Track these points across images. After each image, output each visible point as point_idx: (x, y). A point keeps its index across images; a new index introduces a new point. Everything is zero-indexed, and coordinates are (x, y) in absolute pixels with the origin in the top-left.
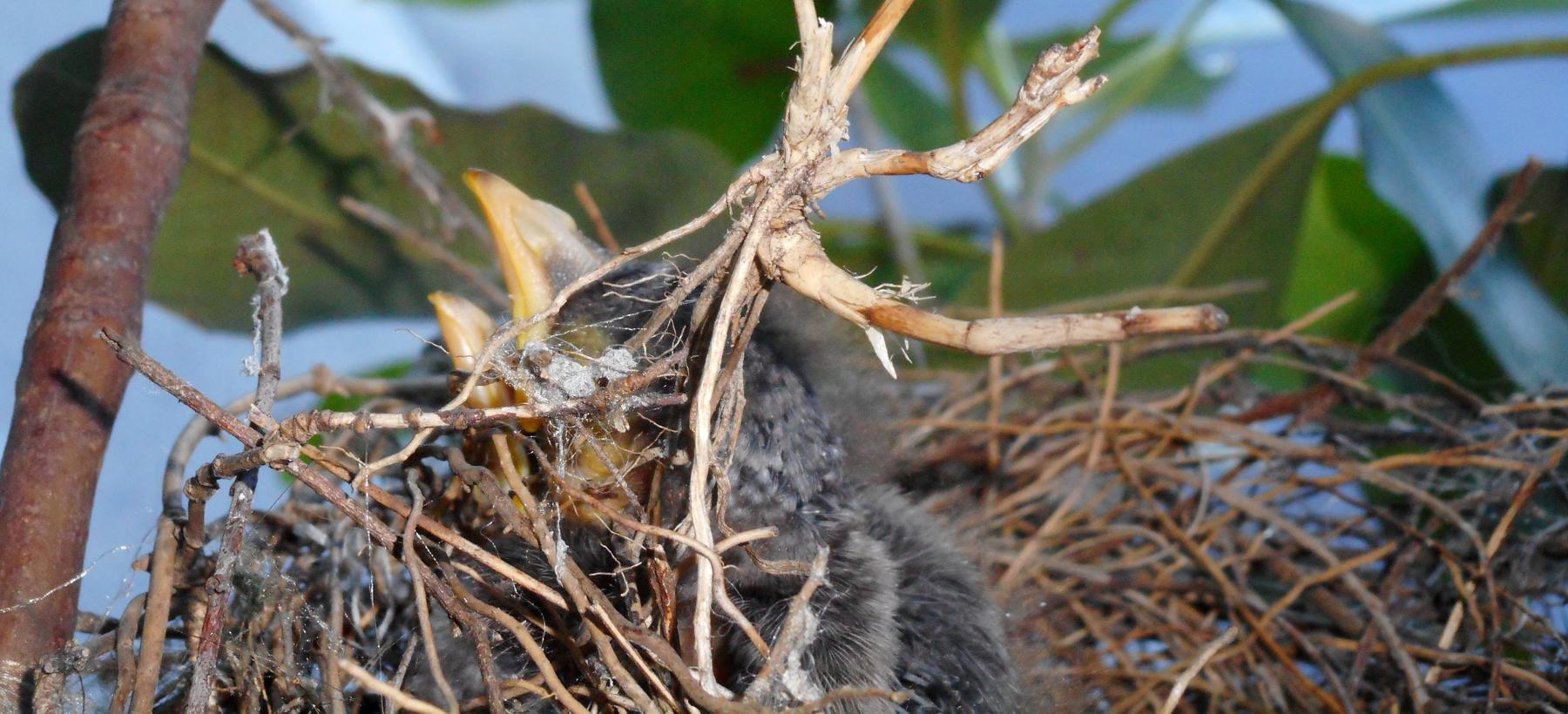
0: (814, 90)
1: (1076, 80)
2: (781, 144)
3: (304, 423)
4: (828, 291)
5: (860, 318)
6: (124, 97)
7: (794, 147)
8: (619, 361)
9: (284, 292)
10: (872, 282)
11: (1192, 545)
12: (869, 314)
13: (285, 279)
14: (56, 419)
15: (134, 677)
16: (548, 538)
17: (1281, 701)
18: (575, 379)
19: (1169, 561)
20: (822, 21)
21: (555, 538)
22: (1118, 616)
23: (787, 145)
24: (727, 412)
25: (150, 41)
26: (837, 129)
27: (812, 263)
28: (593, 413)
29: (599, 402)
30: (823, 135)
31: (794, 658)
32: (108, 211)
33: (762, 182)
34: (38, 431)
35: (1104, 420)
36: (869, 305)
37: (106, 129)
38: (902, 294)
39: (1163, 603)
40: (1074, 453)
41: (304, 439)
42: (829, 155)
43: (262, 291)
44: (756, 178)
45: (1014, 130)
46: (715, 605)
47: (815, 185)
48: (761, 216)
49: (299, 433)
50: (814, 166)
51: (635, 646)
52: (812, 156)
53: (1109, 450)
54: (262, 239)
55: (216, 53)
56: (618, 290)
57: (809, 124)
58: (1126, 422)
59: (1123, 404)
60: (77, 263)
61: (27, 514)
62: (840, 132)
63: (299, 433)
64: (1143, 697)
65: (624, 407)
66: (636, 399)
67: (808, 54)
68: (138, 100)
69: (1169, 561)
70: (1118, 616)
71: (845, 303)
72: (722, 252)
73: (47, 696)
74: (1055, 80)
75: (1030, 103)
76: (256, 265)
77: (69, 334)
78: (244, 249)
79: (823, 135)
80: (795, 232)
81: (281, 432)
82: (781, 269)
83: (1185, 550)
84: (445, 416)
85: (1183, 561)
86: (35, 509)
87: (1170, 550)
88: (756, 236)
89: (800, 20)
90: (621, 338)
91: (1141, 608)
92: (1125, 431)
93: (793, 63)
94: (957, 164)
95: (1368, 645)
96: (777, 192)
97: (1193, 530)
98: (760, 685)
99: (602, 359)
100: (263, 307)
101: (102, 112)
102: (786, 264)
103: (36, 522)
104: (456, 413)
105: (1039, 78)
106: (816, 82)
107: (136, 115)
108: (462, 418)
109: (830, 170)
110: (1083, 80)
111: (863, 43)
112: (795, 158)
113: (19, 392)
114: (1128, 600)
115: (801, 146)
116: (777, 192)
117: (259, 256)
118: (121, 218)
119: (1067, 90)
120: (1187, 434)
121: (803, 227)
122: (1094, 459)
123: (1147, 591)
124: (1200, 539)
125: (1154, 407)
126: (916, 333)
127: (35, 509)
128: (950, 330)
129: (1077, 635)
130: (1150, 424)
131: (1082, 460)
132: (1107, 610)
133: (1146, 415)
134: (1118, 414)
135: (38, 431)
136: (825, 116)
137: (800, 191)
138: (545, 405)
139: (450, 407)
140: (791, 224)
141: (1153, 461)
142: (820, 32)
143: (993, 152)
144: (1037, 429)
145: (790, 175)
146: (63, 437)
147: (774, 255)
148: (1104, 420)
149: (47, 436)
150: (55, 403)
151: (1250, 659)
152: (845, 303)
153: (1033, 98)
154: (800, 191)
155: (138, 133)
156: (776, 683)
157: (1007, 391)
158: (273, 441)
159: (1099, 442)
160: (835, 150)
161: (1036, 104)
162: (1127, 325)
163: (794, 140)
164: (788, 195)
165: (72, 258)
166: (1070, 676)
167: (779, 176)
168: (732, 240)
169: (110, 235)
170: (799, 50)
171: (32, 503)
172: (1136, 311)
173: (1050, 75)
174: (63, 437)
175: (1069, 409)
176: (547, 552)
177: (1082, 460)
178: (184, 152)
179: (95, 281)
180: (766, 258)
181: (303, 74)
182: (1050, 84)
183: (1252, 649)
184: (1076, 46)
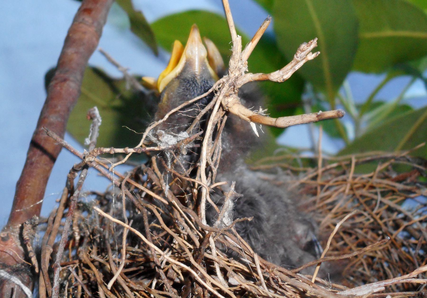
0: (236, 55)
1: (311, 53)
2: (228, 72)
3: (96, 151)
4: (240, 112)
5: (248, 119)
6: (62, 75)
7: (232, 73)
8: (184, 135)
9: (99, 124)
10: (252, 110)
11: (375, 216)
12: (250, 118)
13: (100, 120)
14: (37, 160)
15: (52, 227)
16: (164, 184)
17: (397, 259)
18: (172, 141)
19: (368, 220)
20: (238, 36)
21: (166, 185)
22: (354, 237)
23: (230, 72)
24: (216, 152)
25: (70, 60)
26: (244, 68)
27: (236, 105)
28: (177, 150)
29: (178, 146)
30: (240, 69)
31: (226, 214)
32: (56, 106)
33: (223, 83)
34: (32, 164)
35: (350, 180)
36: (251, 115)
37: (57, 84)
38: (259, 113)
39: (367, 233)
40: (341, 190)
41: (96, 156)
42: (242, 75)
43: (93, 123)
44: (221, 82)
45: (293, 67)
46: (207, 201)
47: (237, 83)
48: (222, 92)
49: (95, 154)
50: (237, 78)
51: (185, 213)
52: (237, 75)
53: (352, 189)
54: (95, 110)
55: (98, 72)
56: (182, 113)
57: (235, 65)
58: (356, 180)
59: (356, 175)
60: (46, 120)
61: (27, 185)
62: (245, 68)
63: (95, 154)
64: (360, 260)
65: (185, 147)
66: (188, 145)
67: (234, 45)
68: (66, 76)
69: (368, 220)
70: (354, 237)
71: (244, 115)
72: (212, 103)
73: (27, 230)
74: (304, 52)
75: (297, 59)
76: (92, 116)
77: (42, 138)
78: (90, 112)
79: (240, 69)
80: (232, 97)
81: (90, 154)
82: (228, 107)
83: (372, 217)
84: (135, 150)
85: (372, 220)
86: (29, 184)
87: (368, 217)
88: (221, 98)
89: (232, 35)
90: (186, 129)
91: (360, 234)
92: (356, 184)
93: (231, 48)
94: (277, 76)
95: (421, 241)
96: (227, 85)
97: (375, 211)
98: (218, 222)
99: (179, 135)
100: (93, 127)
101: (56, 79)
102: (229, 106)
103: (29, 188)
104: (138, 148)
105: (299, 51)
106: (237, 53)
107: (65, 80)
108: (139, 150)
109: (242, 79)
110: (313, 53)
111: (251, 43)
112: (232, 75)
113: (28, 153)
114: (356, 232)
115: (233, 72)
116: (227, 85)
117: (94, 114)
118: (59, 108)
119: (308, 56)
120: (375, 185)
121: (234, 96)
122: (347, 191)
123: (362, 229)
124: (377, 214)
125: (365, 176)
126: (263, 122)
127: (29, 184)
128: (272, 120)
129: (341, 243)
130: (364, 181)
131: (344, 191)
132: (350, 234)
133: (362, 179)
134: (354, 178)
135: (32, 164)
136: (240, 63)
137: (233, 85)
138: (162, 147)
139: (137, 147)
140: (231, 94)
141: (364, 191)
142: (237, 38)
143: (287, 73)
144: (331, 183)
145: (230, 80)
146: (39, 165)
147: (226, 103)
148: (350, 180)
149: (34, 165)
150: (37, 156)
151: (390, 248)
152: (244, 115)
153: (298, 58)
154: (233, 85)
155: (65, 85)
156: (222, 221)
157: (323, 172)
158: (88, 156)
159: (348, 187)
160: (243, 73)
161: (299, 59)
162: (318, 116)
163: (232, 70)
164: (230, 86)
165: (45, 118)
166: (223, 141)
167: (227, 81)
168: (214, 99)
169: (56, 112)
170: (232, 44)
171: (29, 182)
172: (320, 112)
173: (303, 51)
174: (39, 165)
175: (341, 178)
176: (163, 188)
177: (344, 191)
178: (79, 91)
179: (51, 124)
180: (224, 104)
181: (124, 80)
182: (303, 54)
183: (390, 245)
184: (310, 42)
